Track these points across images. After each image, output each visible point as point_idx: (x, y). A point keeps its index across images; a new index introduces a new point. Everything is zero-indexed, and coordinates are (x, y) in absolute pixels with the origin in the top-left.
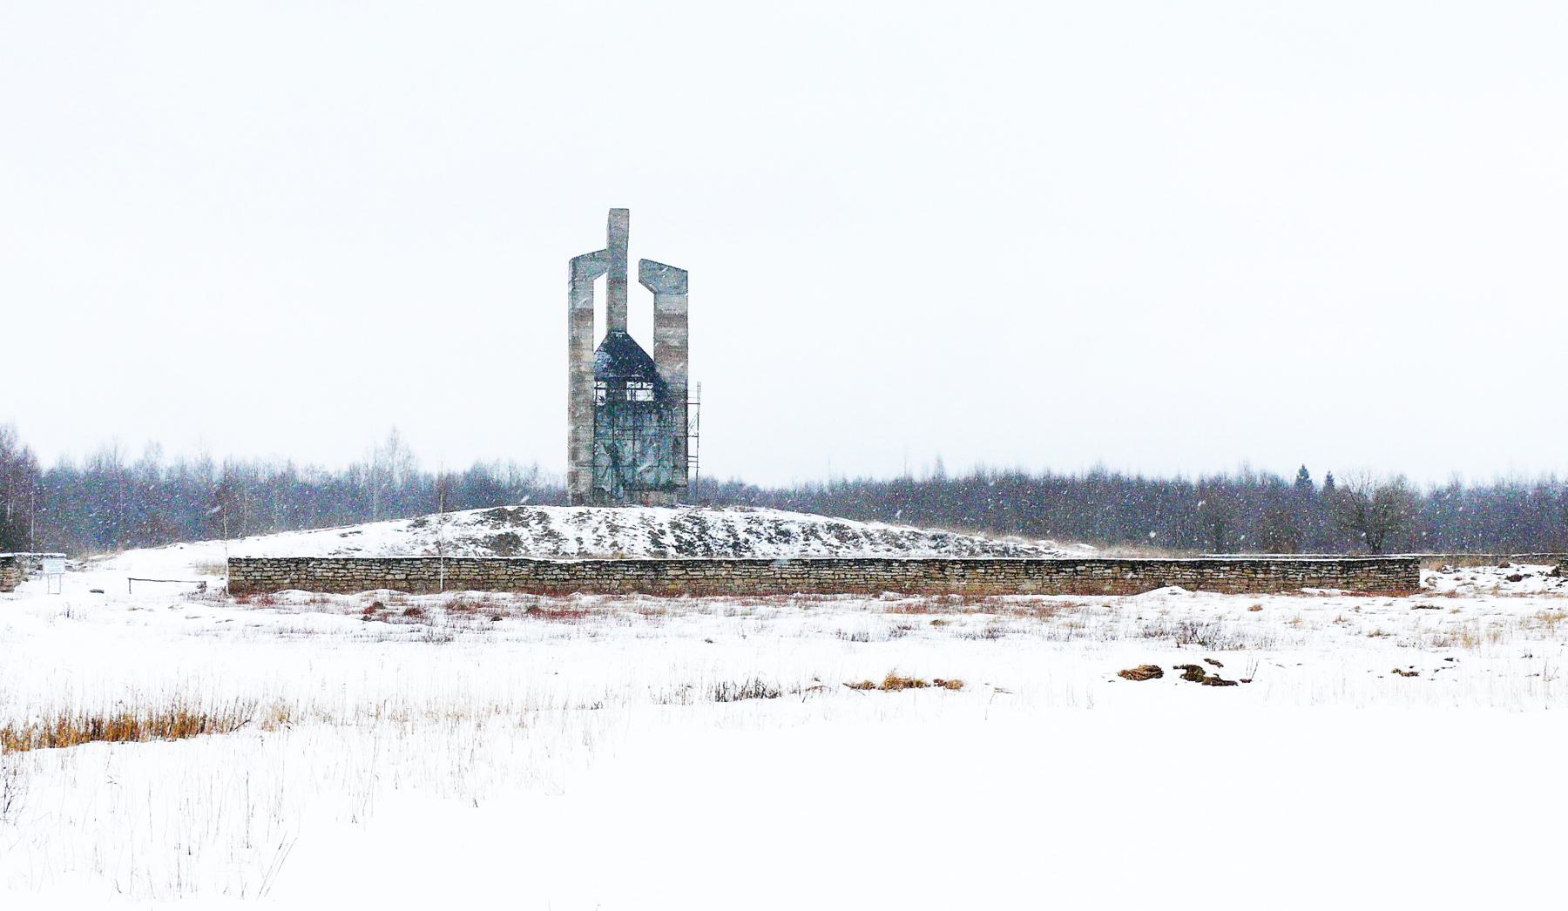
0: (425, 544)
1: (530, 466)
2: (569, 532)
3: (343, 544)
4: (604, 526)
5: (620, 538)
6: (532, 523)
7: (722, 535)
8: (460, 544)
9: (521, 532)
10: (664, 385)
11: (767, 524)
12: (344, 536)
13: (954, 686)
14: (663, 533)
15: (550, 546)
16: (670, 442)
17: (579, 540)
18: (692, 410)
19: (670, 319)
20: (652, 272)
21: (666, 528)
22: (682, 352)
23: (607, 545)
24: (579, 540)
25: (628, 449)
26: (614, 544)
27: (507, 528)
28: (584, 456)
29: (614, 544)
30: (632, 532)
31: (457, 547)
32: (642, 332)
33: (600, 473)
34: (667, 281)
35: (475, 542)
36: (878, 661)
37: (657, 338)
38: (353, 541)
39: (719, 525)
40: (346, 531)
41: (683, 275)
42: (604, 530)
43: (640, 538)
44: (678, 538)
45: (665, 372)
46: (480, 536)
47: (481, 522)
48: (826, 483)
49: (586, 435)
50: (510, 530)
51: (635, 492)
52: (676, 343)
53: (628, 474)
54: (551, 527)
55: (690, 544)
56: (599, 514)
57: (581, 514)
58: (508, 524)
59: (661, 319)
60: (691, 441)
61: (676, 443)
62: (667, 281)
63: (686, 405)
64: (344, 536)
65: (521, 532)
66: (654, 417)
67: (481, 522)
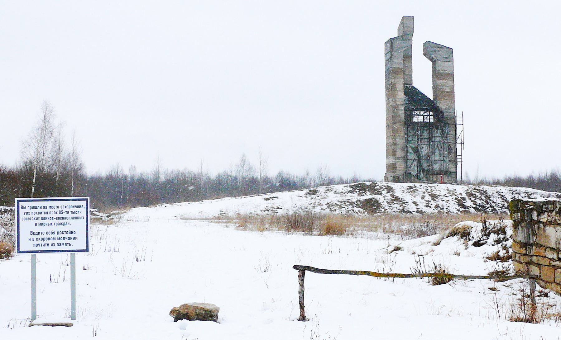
0: (320, 204)
1: (238, 161)
2: (407, 197)
3: (269, 204)
4: (427, 195)
5: (440, 202)
6: (384, 192)
7: (499, 201)
8: (343, 205)
9: (378, 197)
10: (442, 113)
11: (523, 195)
12: (267, 199)
13: (208, 315)
14: (464, 199)
15: (398, 206)
16: (446, 145)
17: (415, 203)
18: (459, 128)
19: (443, 75)
20: (433, 51)
21: (464, 195)
22: (451, 95)
23: (433, 206)
24: (415, 203)
25: (425, 150)
26: (437, 206)
27: (368, 196)
28: (400, 154)
29: (437, 206)
30: (446, 199)
31: (341, 207)
32: (423, 83)
33: (409, 164)
34: (438, 54)
35: (352, 204)
36: (492, 286)
37: (435, 88)
38: (276, 203)
39: (496, 194)
40: (268, 196)
41: (450, 51)
42: (428, 197)
43: (451, 202)
44: (475, 203)
45: (442, 106)
46: (354, 200)
47: (350, 192)
48: (129, 176)
49: (401, 142)
50: (371, 197)
51: (429, 175)
52: (448, 89)
53: (425, 165)
54: (396, 195)
55: (483, 206)
56: (422, 187)
57: (411, 187)
58: (368, 193)
59: (437, 74)
60: (459, 146)
61: (450, 148)
62: (438, 54)
63: (456, 124)
64: (267, 199)
65: (378, 197)
66: (439, 131)
67: (350, 192)
